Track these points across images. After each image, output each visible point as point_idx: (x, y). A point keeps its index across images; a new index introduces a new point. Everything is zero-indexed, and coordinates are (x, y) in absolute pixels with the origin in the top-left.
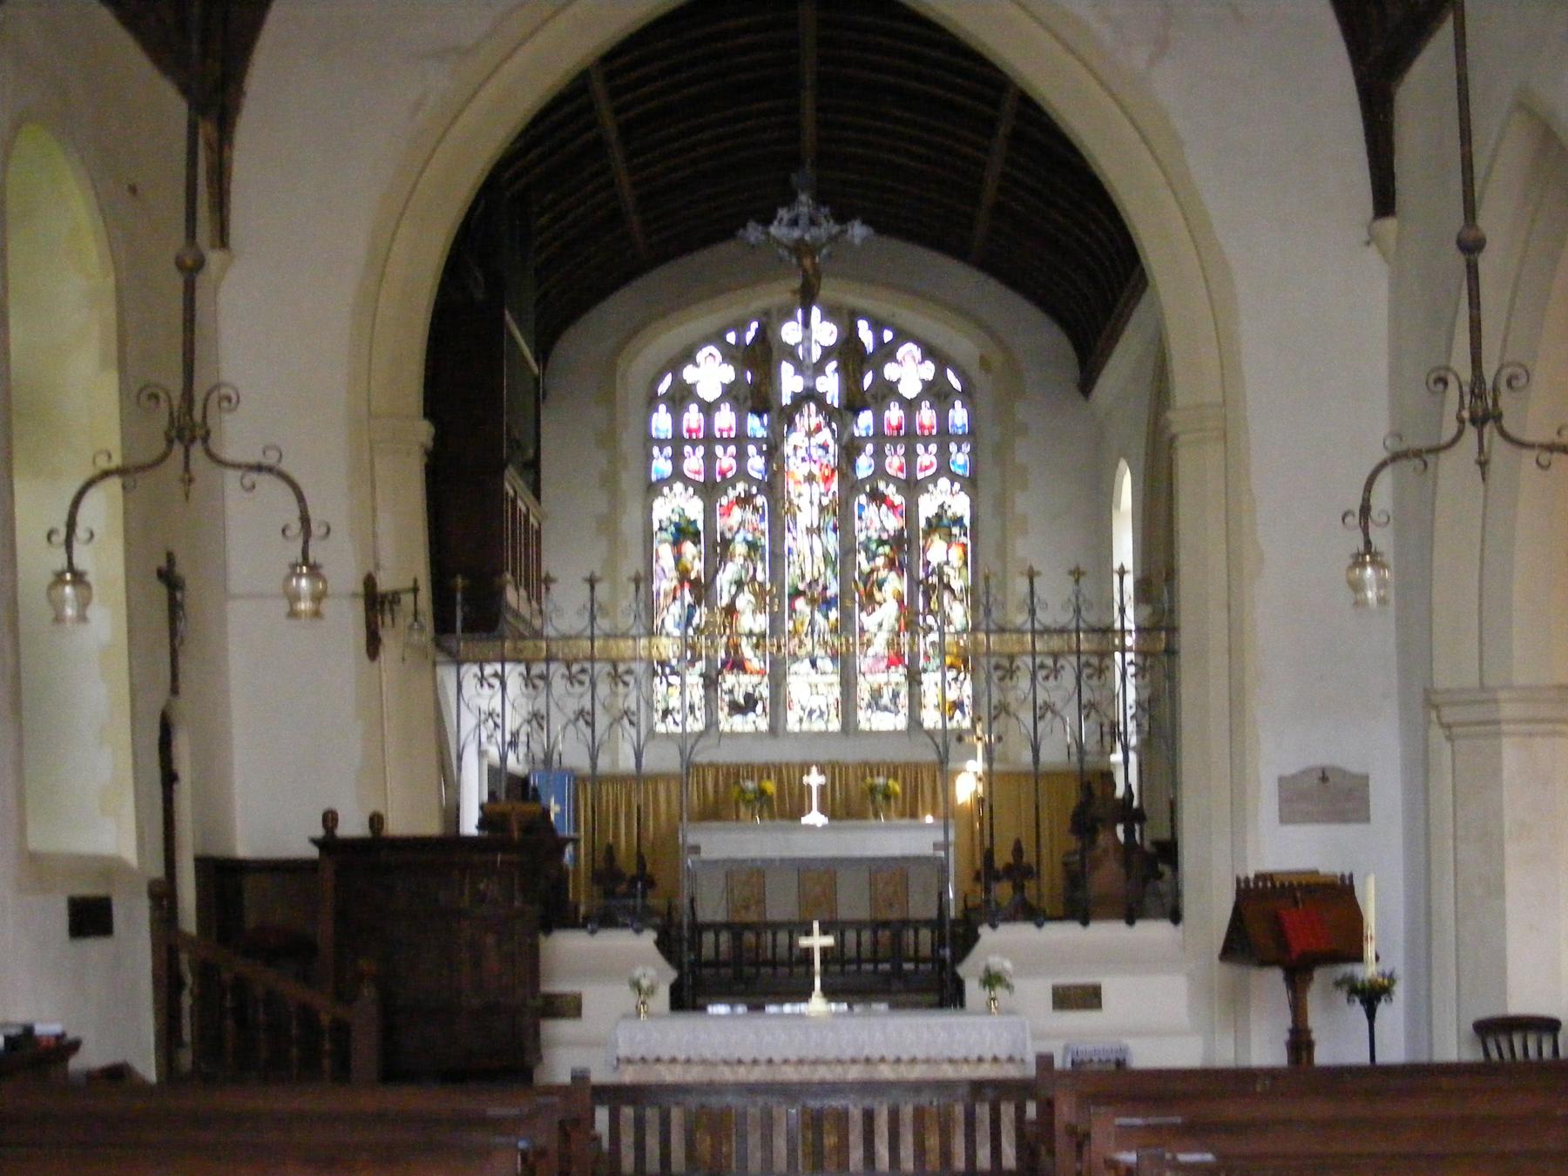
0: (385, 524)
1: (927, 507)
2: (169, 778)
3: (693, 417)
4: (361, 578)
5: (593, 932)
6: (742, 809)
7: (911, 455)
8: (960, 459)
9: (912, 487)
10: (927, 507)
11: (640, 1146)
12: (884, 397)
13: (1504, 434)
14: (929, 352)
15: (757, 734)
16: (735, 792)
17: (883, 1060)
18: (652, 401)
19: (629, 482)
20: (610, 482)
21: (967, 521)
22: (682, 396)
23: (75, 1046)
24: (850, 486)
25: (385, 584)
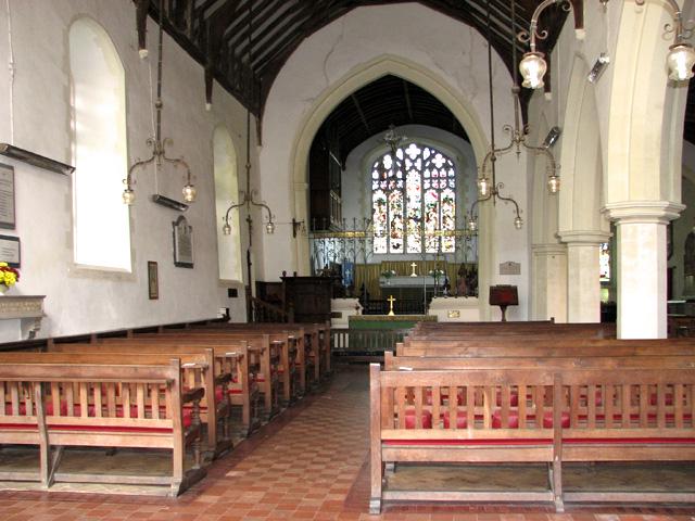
0: (297, 206)
1: (443, 196)
2: (249, 264)
3: (435, 172)
7: (439, 183)
8: (452, 183)
9: (439, 191)
10: (443, 196)
14: (444, 156)
18: (373, 169)
20: (362, 190)
24: (424, 191)
25: (297, 221)
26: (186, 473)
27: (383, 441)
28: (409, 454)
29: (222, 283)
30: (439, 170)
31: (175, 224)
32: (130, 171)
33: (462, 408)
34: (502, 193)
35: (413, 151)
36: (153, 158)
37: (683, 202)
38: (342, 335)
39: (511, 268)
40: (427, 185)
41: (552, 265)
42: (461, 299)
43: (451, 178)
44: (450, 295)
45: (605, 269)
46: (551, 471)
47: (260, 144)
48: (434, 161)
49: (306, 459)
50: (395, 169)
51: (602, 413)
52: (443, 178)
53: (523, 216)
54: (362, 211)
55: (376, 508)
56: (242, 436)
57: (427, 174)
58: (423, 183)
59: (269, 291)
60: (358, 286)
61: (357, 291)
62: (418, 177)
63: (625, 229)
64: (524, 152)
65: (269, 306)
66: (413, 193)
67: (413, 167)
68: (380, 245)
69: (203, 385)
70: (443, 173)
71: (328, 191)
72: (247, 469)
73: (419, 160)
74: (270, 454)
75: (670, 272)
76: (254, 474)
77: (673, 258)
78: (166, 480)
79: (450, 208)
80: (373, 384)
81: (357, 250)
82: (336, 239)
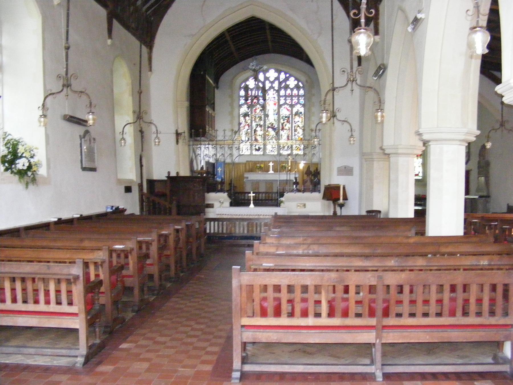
1: (295, 110)
2: (141, 166)
3: (289, 92)
4: (175, 130)
5: (216, 193)
6: (257, 170)
7: (292, 100)
8: (302, 101)
9: (292, 106)
10: (295, 110)
11: (223, 228)
12: (287, 88)
13: (337, 119)
14: (296, 79)
15: (260, 155)
16: (255, 166)
17: (261, 215)
18: (240, 88)
19: (235, 105)
20: (231, 105)
21: (303, 113)
22: (246, 88)
23: (125, 210)
24: (280, 106)
25: (179, 131)
26: (90, 348)
27: (243, 326)
28: (264, 336)
29: (120, 181)
30: (292, 90)
31: (81, 138)
32: (45, 98)
33: (305, 296)
34: (339, 116)
35: (272, 74)
36: (62, 90)
37: (479, 128)
38: (216, 223)
39: (346, 171)
40: (282, 101)
41: (378, 166)
42: (307, 194)
43: (302, 96)
44: (299, 191)
45: (419, 170)
46: (373, 349)
47: (151, 70)
48: (288, 83)
49: (182, 332)
50: (257, 88)
51: (414, 299)
52: (295, 96)
53: (356, 134)
54: (231, 123)
55: (236, 379)
56: (133, 311)
57: (282, 92)
58: (279, 100)
59: (158, 188)
60: (227, 181)
61: (226, 187)
62: (276, 96)
63: (434, 148)
64: (357, 90)
65: (157, 200)
66: (271, 108)
67: (272, 87)
68: (245, 149)
69: (102, 277)
70: (295, 92)
71: (204, 107)
72: (136, 342)
73: (277, 83)
74: (154, 328)
75: (468, 173)
76: (142, 346)
77: (470, 162)
78: (73, 352)
79: (300, 120)
80: (235, 283)
81: (226, 155)
82: (210, 146)
